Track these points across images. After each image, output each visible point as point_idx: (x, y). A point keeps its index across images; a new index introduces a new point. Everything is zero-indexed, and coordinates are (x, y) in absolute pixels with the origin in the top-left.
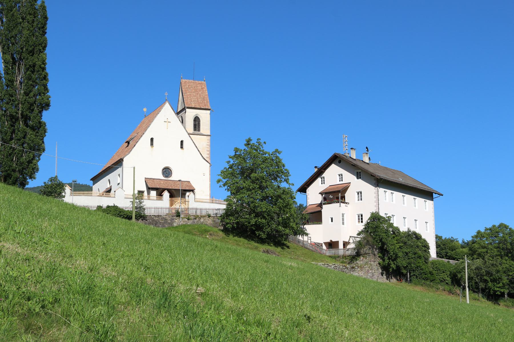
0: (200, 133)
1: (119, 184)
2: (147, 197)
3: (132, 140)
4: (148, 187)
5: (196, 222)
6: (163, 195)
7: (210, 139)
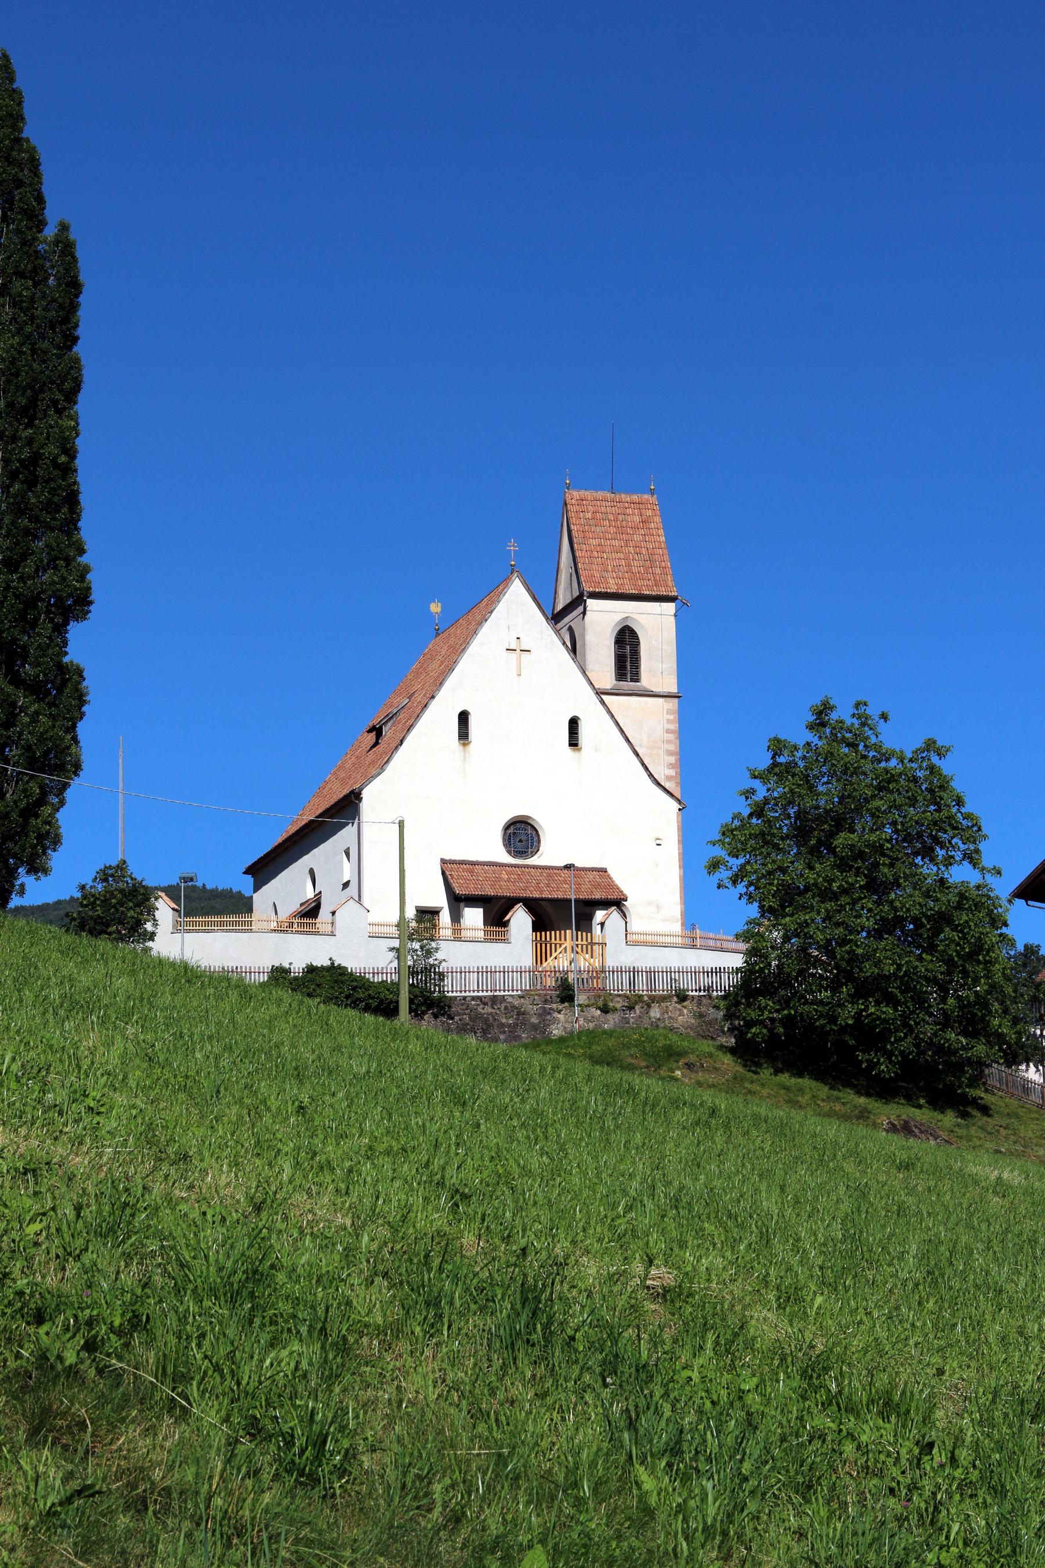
1: (346, 885)
3: (391, 722)
4: (454, 893)
5: (632, 1020)
6: (509, 920)
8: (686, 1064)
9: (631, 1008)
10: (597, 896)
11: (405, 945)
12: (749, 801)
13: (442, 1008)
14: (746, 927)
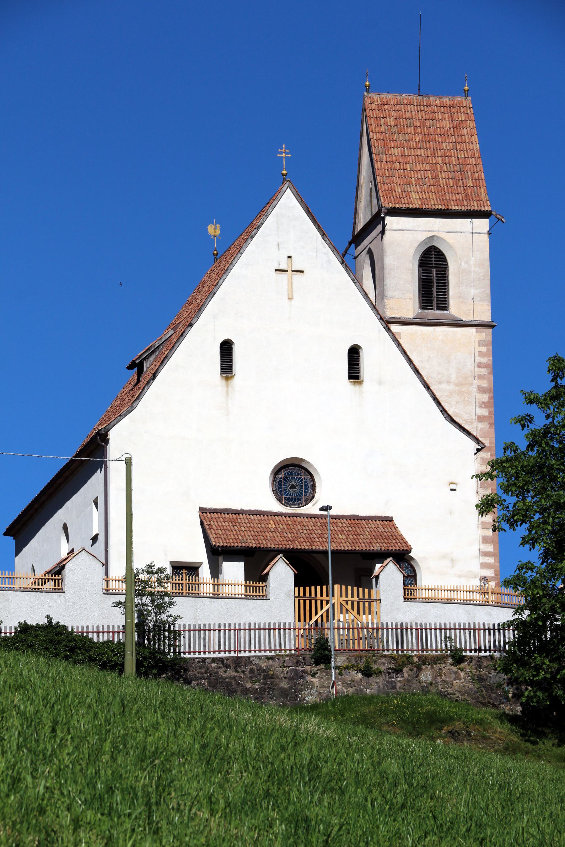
0: (450, 314)
1: (95, 539)
2: (209, 589)
3: (154, 356)
4: (211, 545)
5: (399, 685)
6: (268, 574)
7: (490, 338)
8: (450, 732)
9: (398, 671)
10: (377, 547)
11: (132, 600)
12: (527, 431)
13: (178, 672)
14: (518, 572)
